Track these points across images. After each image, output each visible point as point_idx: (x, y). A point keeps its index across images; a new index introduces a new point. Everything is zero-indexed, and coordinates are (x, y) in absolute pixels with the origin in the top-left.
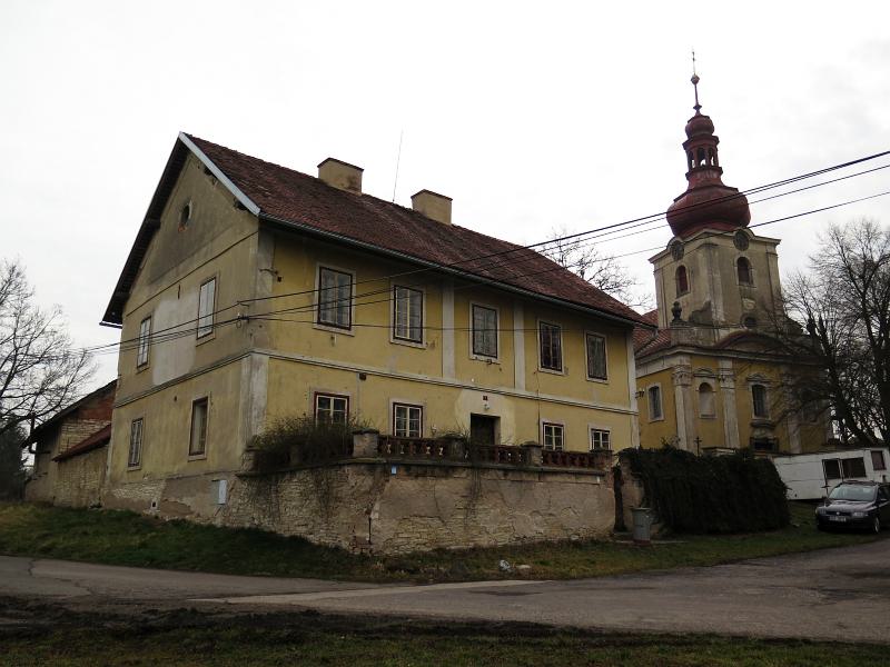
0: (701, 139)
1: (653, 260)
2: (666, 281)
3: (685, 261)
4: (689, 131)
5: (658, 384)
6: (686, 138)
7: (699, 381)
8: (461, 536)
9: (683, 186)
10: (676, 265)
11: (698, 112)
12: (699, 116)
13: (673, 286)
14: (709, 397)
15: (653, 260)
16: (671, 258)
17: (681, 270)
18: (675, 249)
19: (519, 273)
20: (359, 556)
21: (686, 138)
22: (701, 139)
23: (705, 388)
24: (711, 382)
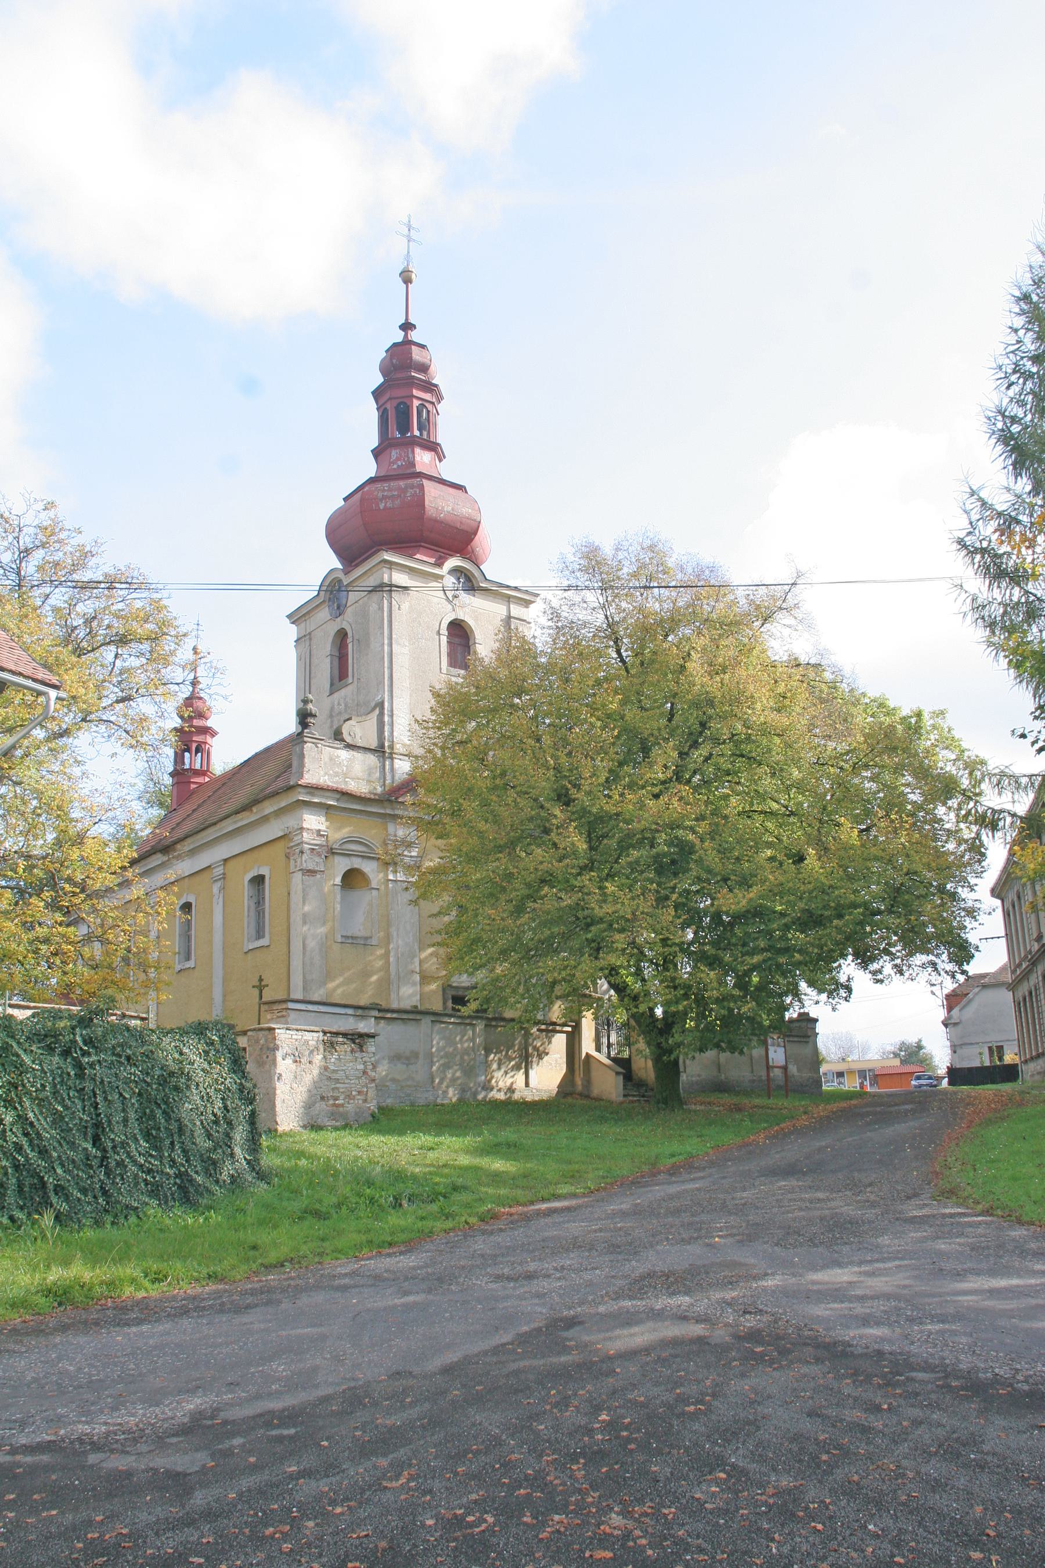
0: (404, 391)
1: (297, 617)
2: (315, 661)
3: (346, 622)
4: (386, 369)
5: (264, 871)
6: (381, 380)
7: (342, 865)
8: (726, 797)
9: (376, 444)
10: (333, 628)
11: (406, 336)
12: (407, 343)
13: (324, 668)
14: (364, 899)
15: (297, 617)
16: (324, 614)
17: (342, 636)
18: (333, 592)
19: (216, 1491)
20: (939, 854)
21: (381, 380)
22: (404, 391)
23: (352, 879)
24: (369, 868)
